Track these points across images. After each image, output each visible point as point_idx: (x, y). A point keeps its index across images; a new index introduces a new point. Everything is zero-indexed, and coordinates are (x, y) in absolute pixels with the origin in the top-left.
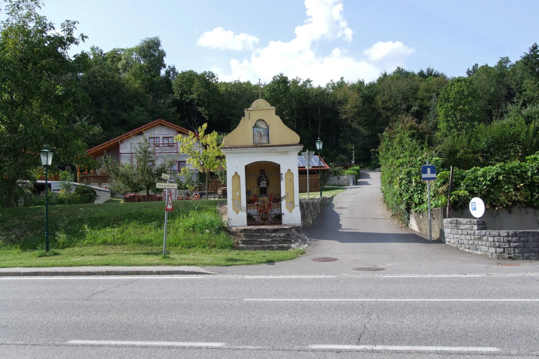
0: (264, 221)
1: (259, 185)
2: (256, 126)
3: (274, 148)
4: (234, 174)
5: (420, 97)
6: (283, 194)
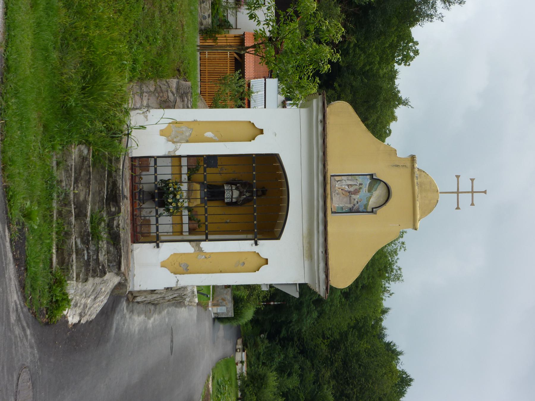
0: (138, 195)
1: (227, 183)
2: (374, 180)
3: (321, 228)
4: (259, 126)
5: (346, 199)
6: (207, 246)
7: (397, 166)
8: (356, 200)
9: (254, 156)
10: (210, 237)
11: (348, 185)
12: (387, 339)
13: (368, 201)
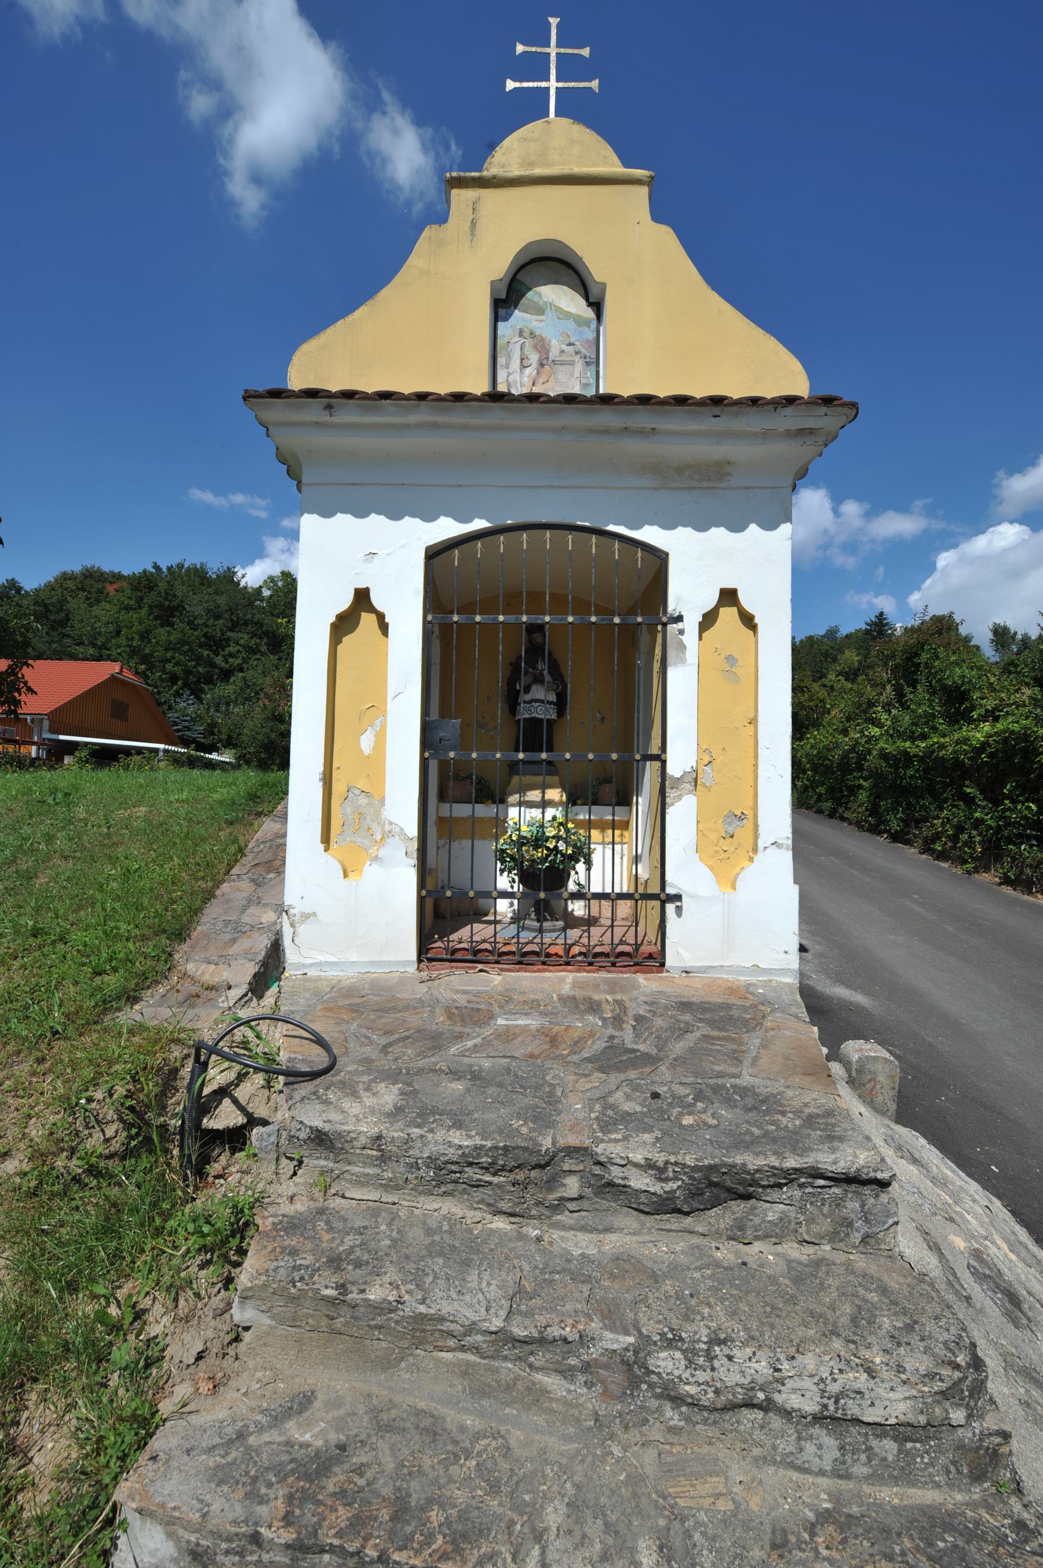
4: (345, 602)
6: (681, 755)
7: (473, 223)
8: (564, 347)
9: (430, 618)
10: (654, 749)
11: (523, 367)
12: (753, 527)
13: (568, 315)
